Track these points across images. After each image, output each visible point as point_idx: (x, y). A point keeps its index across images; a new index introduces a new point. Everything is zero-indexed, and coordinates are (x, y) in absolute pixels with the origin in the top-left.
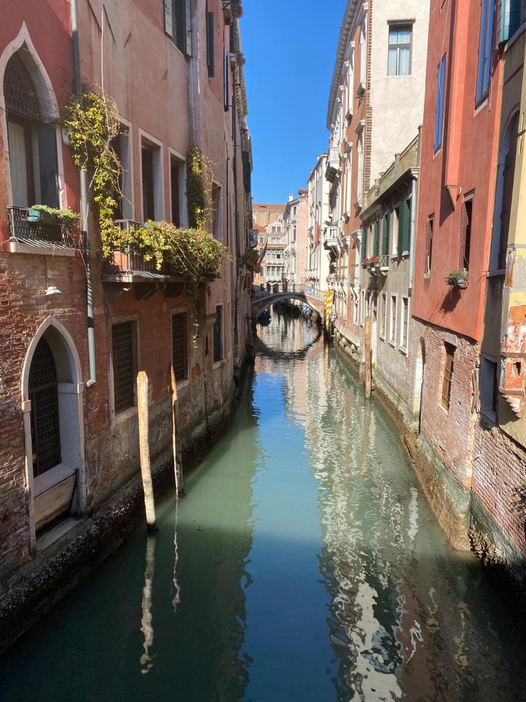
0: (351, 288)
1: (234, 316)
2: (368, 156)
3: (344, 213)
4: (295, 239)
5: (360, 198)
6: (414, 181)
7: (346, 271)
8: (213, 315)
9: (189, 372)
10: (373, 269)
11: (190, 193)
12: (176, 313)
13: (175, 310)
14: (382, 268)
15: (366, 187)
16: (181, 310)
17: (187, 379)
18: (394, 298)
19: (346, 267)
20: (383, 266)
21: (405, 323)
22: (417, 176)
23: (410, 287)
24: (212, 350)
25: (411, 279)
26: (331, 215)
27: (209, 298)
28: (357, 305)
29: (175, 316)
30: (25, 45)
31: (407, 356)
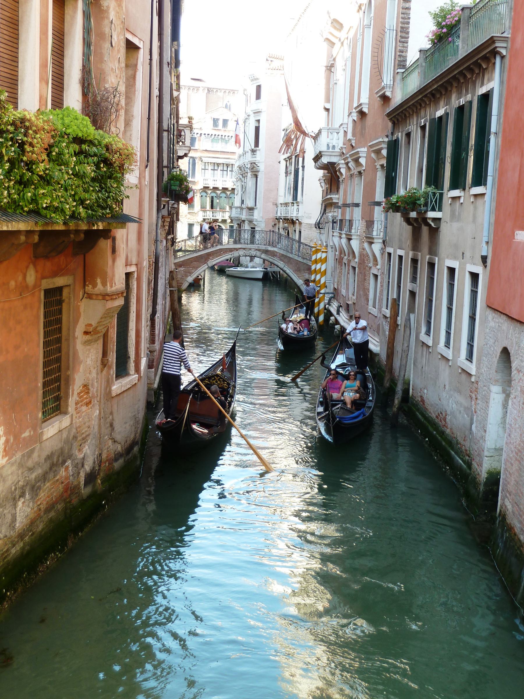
0: (366, 245)
1: (152, 292)
2: (407, 5)
3: (355, 105)
4: (257, 144)
5: (387, 79)
6: (498, 60)
7: (357, 213)
8: (118, 294)
9: (72, 400)
10: (413, 215)
11: (181, 184)
12: (51, 286)
13: (50, 280)
14: (431, 214)
15: (401, 63)
16: (60, 281)
17: (66, 413)
18: (452, 271)
19: (357, 205)
20: (433, 209)
21: (472, 318)
22: (504, 52)
23: (484, 254)
24: (112, 357)
25: (485, 239)
26: (328, 106)
27: (114, 260)
28: (376, 276)
29: (48, 292)
30: (471, 103)
31: (473, 379)
